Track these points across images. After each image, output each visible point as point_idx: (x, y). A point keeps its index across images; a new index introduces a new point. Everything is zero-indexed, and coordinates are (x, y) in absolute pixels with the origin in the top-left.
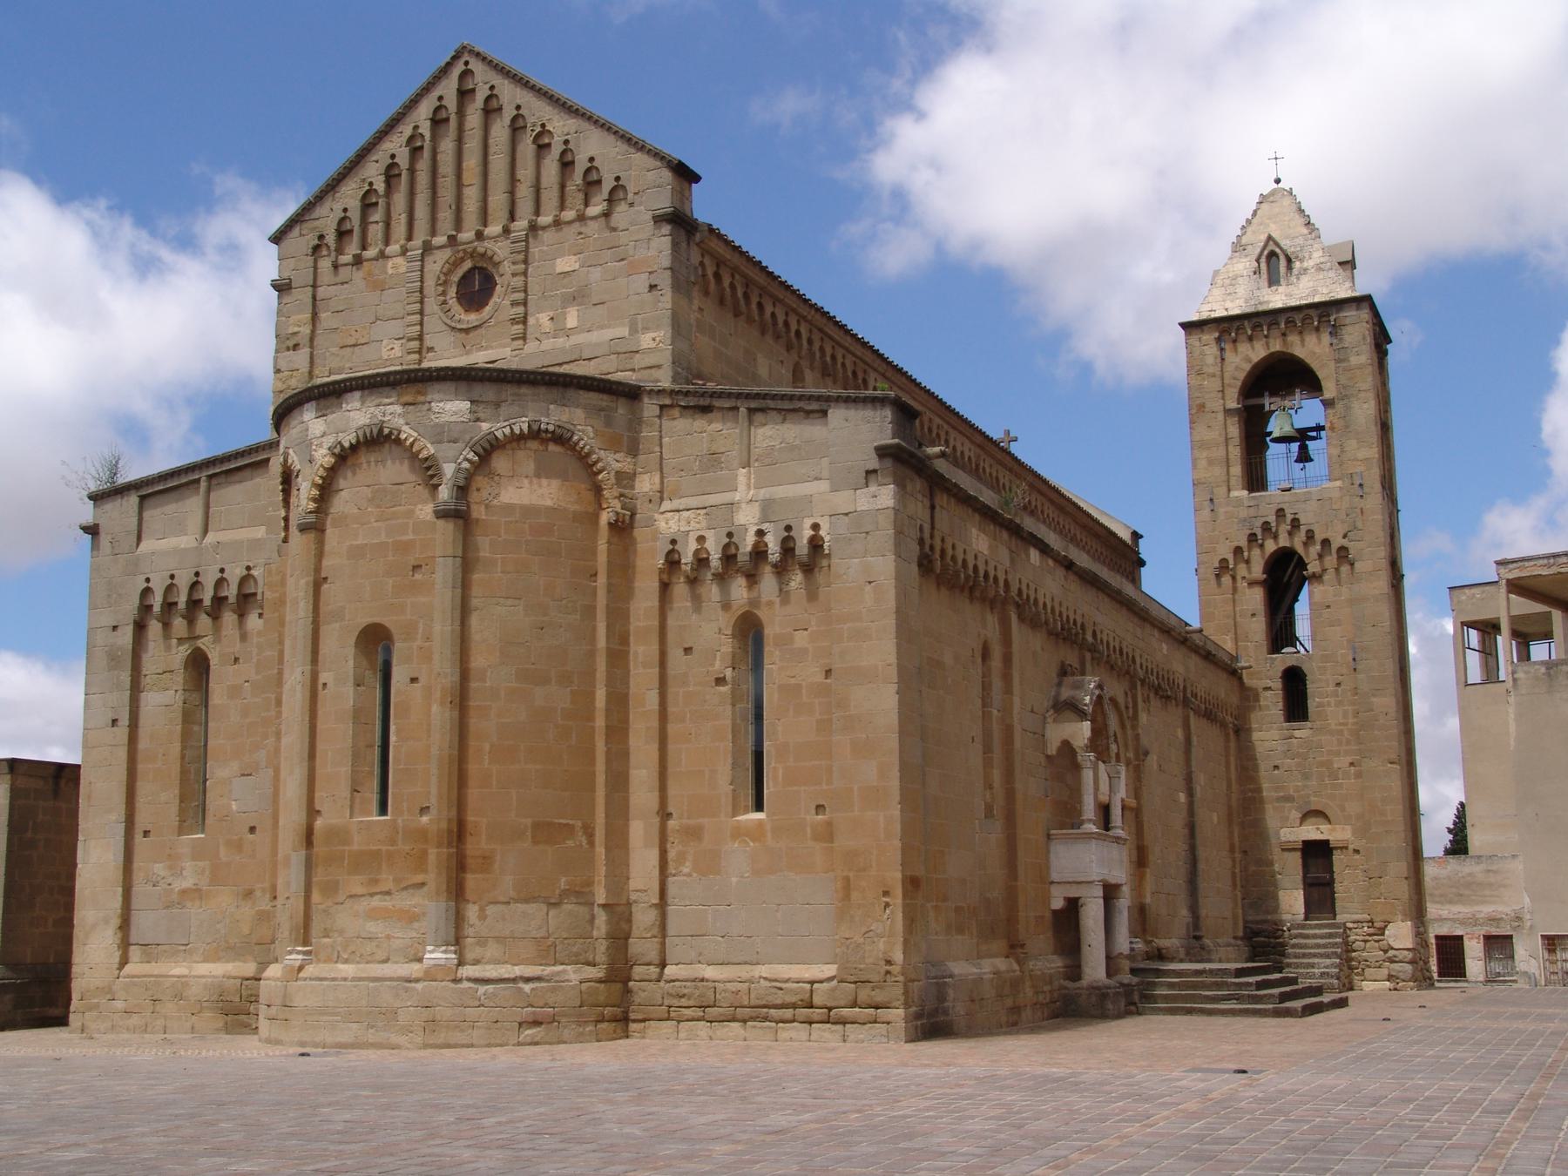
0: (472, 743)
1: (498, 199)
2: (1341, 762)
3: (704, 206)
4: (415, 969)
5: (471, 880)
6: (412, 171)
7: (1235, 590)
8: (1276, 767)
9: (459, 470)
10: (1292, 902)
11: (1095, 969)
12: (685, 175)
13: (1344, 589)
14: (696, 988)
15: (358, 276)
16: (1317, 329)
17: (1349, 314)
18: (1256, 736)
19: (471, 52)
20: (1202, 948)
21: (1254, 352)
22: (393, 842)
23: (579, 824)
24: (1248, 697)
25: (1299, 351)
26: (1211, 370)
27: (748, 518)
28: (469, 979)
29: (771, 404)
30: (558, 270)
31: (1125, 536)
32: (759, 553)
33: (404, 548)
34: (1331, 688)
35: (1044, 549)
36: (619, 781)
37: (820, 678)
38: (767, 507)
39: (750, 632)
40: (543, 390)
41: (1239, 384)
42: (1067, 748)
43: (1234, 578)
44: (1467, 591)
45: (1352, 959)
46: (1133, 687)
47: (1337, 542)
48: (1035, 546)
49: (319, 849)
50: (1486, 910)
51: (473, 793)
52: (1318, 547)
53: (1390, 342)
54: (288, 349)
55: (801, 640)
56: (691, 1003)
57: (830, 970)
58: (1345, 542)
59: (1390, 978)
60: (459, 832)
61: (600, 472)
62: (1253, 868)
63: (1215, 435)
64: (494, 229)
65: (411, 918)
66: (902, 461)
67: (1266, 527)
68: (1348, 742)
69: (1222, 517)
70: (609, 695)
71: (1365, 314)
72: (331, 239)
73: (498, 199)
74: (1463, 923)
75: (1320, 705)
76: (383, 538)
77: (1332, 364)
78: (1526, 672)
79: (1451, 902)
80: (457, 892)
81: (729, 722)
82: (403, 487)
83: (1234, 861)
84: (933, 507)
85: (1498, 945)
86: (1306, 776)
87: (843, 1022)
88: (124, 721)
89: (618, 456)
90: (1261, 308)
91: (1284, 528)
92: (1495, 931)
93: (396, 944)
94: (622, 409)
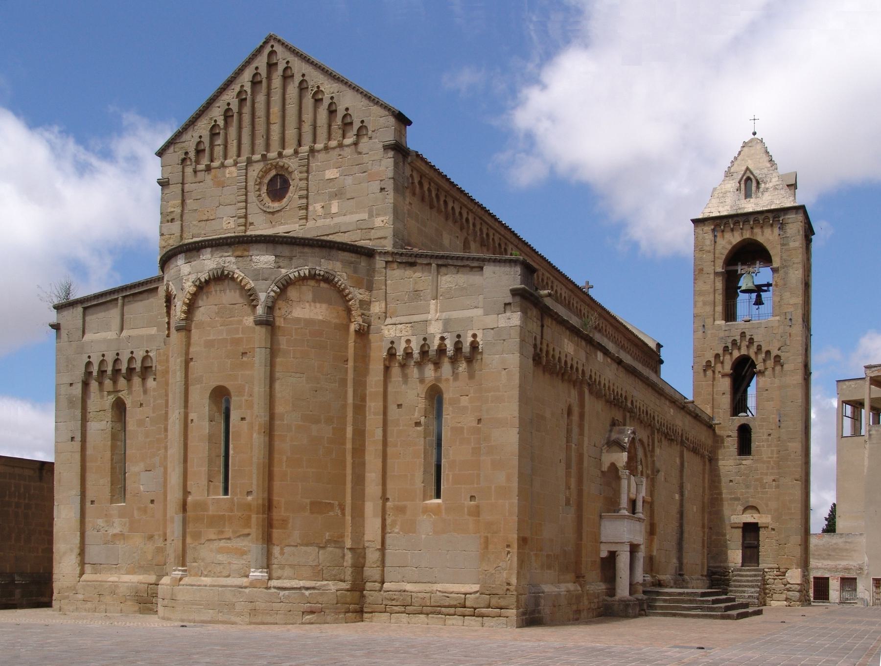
0: (276, 456)
1: (291, 133)
2: (768, 479)
3: (414, 141)
4: (244, 581)
5: (276, 533)
6: (240, 113)
7: (714, 379)
8: (731, 481)
9: (268, 297)
10: (735, 556)
11: (623, 590)
12: (403, 120)
13: (776, 380)
14: (401, 595)
15: (209, 178)
16: (772, 225)
17: (791, 217)
18: (721, 463)
19: (275, 39)
20: (683, 581)
21: (732, 239)
22: (232, 511)
23: (337, 503)
24: (718, 441)
25: (760, 239)
26: (708, 248)
27: (435, 330)
28: (275, 588)
29: (450, 262)
30: (327, 177)
31: (653, 345)
32: (441, 350)
33: (237, 342)
34: (765, 437)
35: (606, 352)
36: (359, 480)
37: (474, 424)
38: (447, 323)
39: (435, 396)
40: (317, 250)
41: (724, 257)
42: (613, 467)
43: (714, 372)
44: (847, 383)
45: (766, 589)
46: (653, 433)
47: (774, 352)
48: (601, 351)
49: (190, 513)
50: (843, 563)
51: (277, 484)
52: (763, 355)
53: (814, 234)
54: (168, 221)
55: (464, 401)
56: (398, 603)
57: (476, 587)
58: (779, 353)
59: (787, 599)
60: (269, 506)
61: (350, 300)
62: (714, 537)
63: (708, 287)
64: (289, 151)
65: (242, 553)
66: (526, 298)
67: (734, 342)
68: (772, 468)
69: (709, 336)
70: (354, 431)
71: (800, 217)
72: (192, 155)
73: (291, 133)
74: (829, 570)
75: (758, 446)
76: (225, 336)
77: (779, 247)
78: (877, 431)
79: (824, 559)
80: (268, 539)
81: (422, 447)
82: (236, 306)
83: (704, 532)
84: (542, 326)
85: (848, 583)
86: (748, 487)
87: (482, 616)
88: (78, 438)
89: (361, 291)
90: (739, 212)
91: (745, 343)
92: (847, 575)
93: (234, 567)
94: (363, 263)
